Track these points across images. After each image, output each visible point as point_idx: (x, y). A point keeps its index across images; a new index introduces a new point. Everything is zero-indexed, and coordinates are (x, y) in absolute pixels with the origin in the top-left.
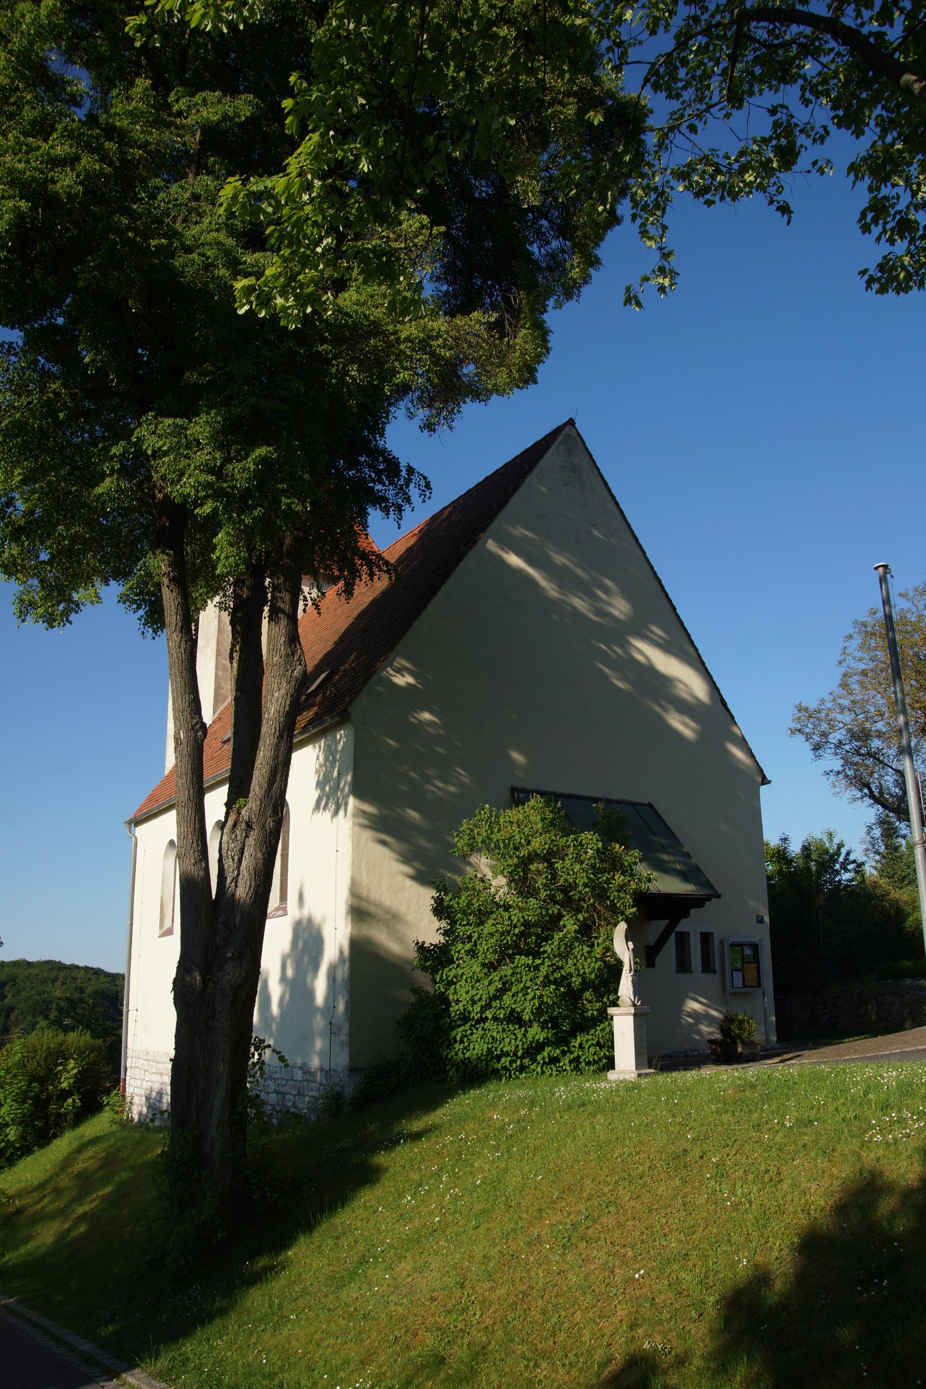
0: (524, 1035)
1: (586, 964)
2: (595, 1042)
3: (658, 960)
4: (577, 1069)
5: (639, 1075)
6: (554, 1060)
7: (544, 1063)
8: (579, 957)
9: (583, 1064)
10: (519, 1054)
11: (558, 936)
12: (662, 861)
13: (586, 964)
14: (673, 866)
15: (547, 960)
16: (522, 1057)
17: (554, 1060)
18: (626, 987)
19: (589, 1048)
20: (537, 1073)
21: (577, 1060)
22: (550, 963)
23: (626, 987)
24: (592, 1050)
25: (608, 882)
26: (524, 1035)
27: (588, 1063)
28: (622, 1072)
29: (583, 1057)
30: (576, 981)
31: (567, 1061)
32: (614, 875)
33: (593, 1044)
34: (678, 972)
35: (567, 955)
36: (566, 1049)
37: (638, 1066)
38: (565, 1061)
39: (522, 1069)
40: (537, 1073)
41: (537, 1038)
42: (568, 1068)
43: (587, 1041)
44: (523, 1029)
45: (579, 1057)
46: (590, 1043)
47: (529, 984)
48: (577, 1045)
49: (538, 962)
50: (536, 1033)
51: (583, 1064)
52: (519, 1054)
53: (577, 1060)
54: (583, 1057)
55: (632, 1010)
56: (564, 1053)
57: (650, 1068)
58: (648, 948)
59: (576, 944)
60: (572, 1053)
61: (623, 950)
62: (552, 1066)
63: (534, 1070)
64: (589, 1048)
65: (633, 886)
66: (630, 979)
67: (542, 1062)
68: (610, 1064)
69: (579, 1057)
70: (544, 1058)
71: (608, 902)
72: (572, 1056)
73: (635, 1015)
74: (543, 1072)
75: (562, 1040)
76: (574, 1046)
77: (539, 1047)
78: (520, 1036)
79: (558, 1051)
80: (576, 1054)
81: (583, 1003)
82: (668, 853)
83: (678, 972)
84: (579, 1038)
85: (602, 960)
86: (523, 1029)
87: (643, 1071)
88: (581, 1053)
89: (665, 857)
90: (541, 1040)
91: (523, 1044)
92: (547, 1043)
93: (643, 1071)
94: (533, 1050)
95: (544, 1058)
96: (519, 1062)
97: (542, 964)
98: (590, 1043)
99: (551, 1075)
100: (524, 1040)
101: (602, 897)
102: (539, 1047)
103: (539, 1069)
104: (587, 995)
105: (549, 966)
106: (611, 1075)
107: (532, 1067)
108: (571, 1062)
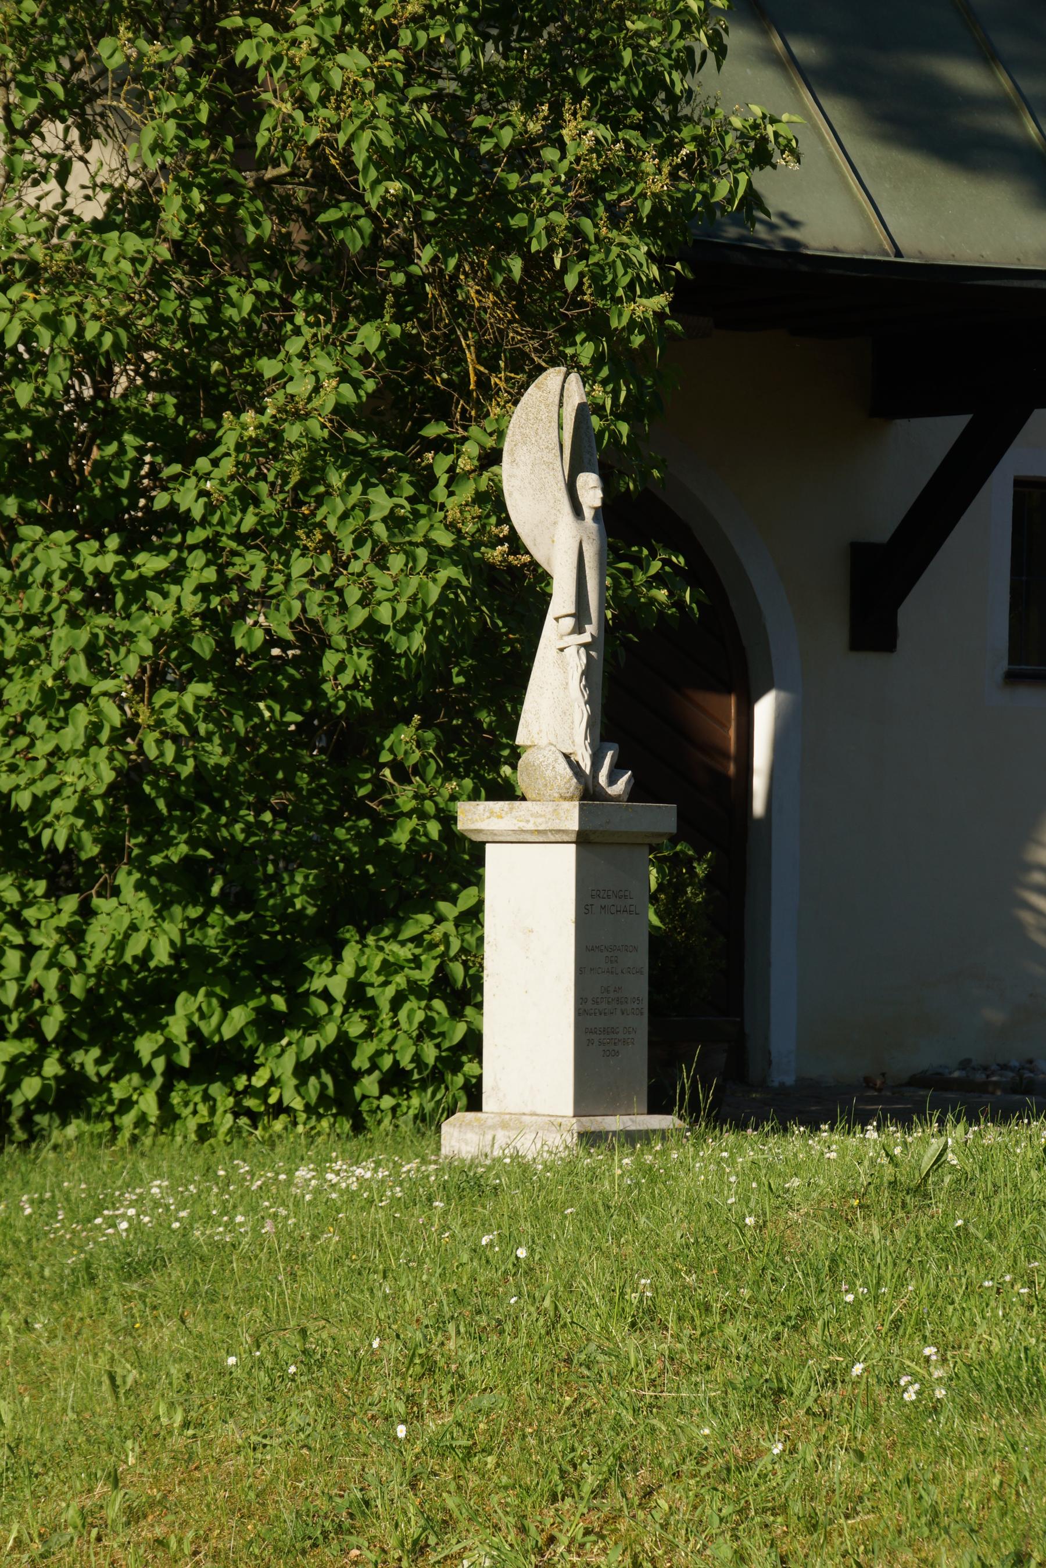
0: (74, 935)
1: (382, 579)
2: (425, 976)
3: (911, 614)
4: (343, 1104)
5: (590, 1139)
6: (218, 1061)
7: (173, 1072)
8: (347, 545)
9: (369, 1084)
10: (51, 1026)
11: (239, 427)
12: (948, 98)
13: (382, 579)
14: (1005, 124)
15: (196, 560)
16: (67, 1041)
17: (218, 1061)
18: (556, 707)
19: (397, 1003)
20: (142, 1121)
21: (337, 1058)
22: (210, 575)
23: (556, 707)
24: (413, 1012)
25: (524, 154)
26: (74, 935)
27: (396, 1080)
28: (510, 1121)
29: (367, 1049)
30: (346, 669)
31: (289, 1062)
32: (556, 122)
33: (414, 989)
34: (1012, 678)
35: (289, 536)
36: (279, 1002)
37: (592, 1088)
38: (278, 1063)
39: (71, 1097)
40: (142, 1121)
41: (135, 947)
42: (298, 1104)
43: (389, 968)
44: (70, 903)
45: (344, 1046)
46: (400, 980)
47: (80, 672)
48: (338, 987)
49: (150, 563)
50: (131, 923)
51: (369, 1084)
52: (51, 1026)
53: (337, 1058)
54: (367, 1049)
55: (570, 817)
56: (270, 1026)
57: (654, 1108)
58: (862, 555)
59: (336, 478)
60: (314, 1024)
61: (545, 501)
62: (216, 1089)
63: (126, 1105)
64: (397, 1003)
65: (656, 180)
66: (576, 661)
67: (159, 1065)
68: (453, 1073)
69: (344, 1046)
70: (168, 1048)
71: (516, 265)
72: (310, 1045)
73: (584, 840)
74: (169, 1117)
75: (270, 964)
76: (326, 995)
77: (148, 994)
78: (46, 938)
79: (240, 1016)
80: (331, 1031)
81: (380, 786)
82: (987, 56)
83: (1012, 678)
84: (350, 954)
85: (461, 554)
86: (70, 903)
87: (615, 1123)
88: (356, 1028)
89: (966, 75)
90: (162, 956)
91: (66, 975)
92: (191, 966)
93: (615, 1123)
94: (119, 1006)
95: (168, 1048)
96: (52, 1067)
97: (175, 574)
98: (400, 980)
99: (204, 1132)
100: (69, 959)
101: (481, 235)
102: (148, 994)
103: (148, 1103)
104: (404, 740)
105: (203, 589)
106: (461, 1138)
107: (119, 1091)
108: (303, 1071)
